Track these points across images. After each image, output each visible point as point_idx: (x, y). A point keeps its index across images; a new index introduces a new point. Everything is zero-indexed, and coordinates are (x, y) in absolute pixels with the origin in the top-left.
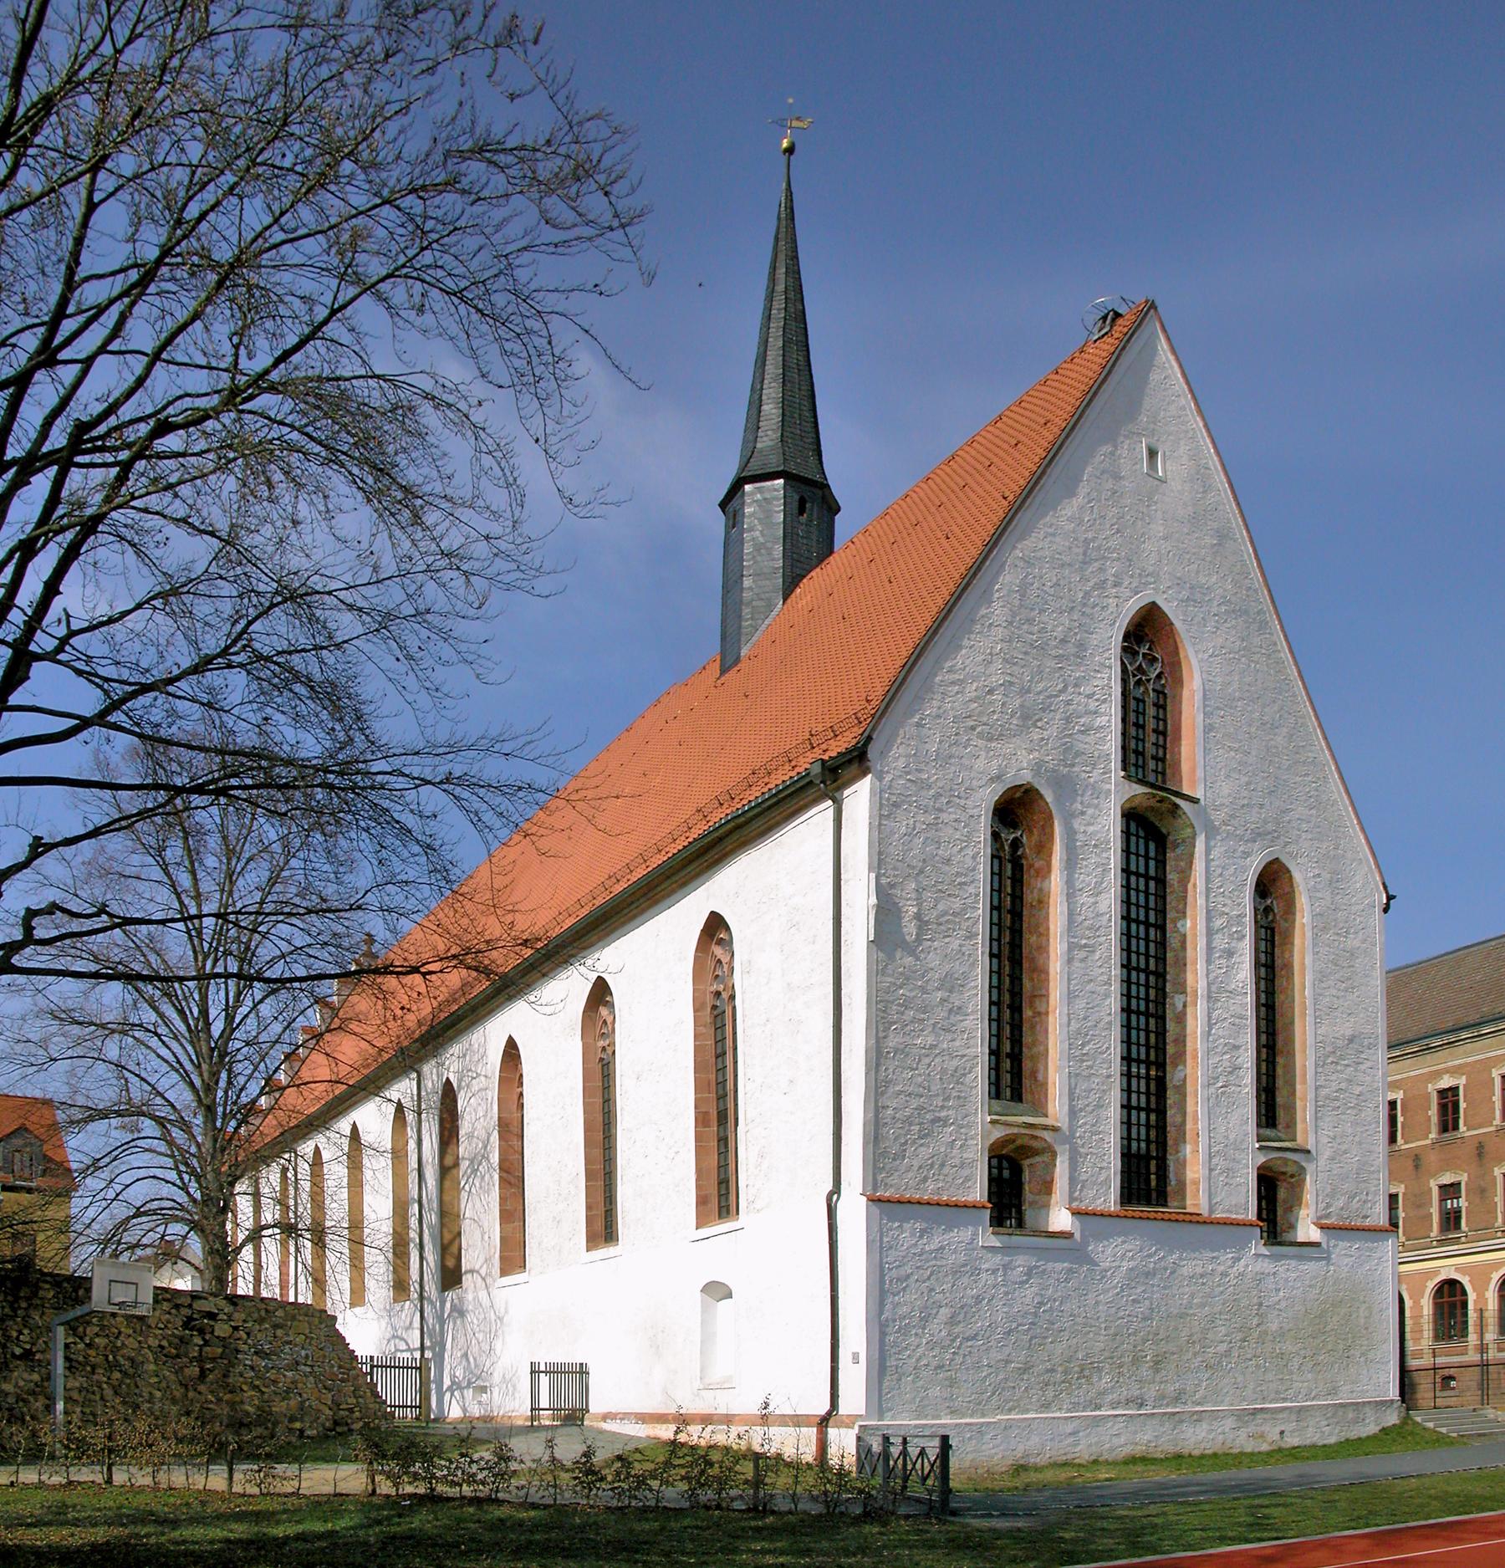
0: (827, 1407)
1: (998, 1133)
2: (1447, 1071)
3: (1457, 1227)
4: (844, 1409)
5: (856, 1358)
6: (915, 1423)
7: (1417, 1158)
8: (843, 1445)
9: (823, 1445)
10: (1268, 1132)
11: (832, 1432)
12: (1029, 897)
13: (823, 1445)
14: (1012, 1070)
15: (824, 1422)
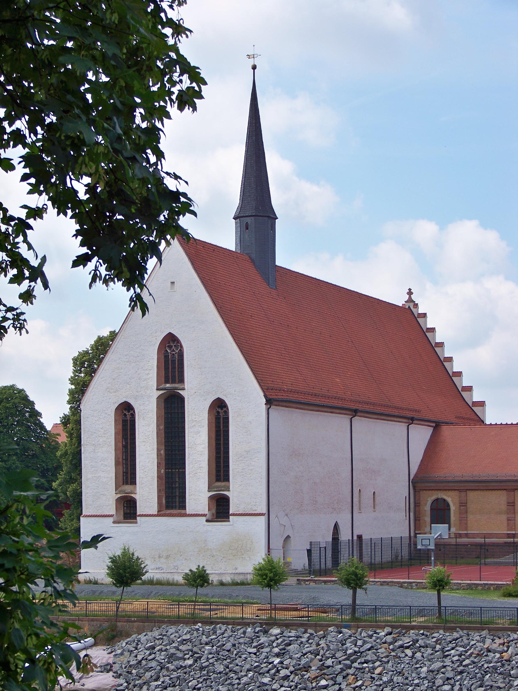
1: (119, 496)
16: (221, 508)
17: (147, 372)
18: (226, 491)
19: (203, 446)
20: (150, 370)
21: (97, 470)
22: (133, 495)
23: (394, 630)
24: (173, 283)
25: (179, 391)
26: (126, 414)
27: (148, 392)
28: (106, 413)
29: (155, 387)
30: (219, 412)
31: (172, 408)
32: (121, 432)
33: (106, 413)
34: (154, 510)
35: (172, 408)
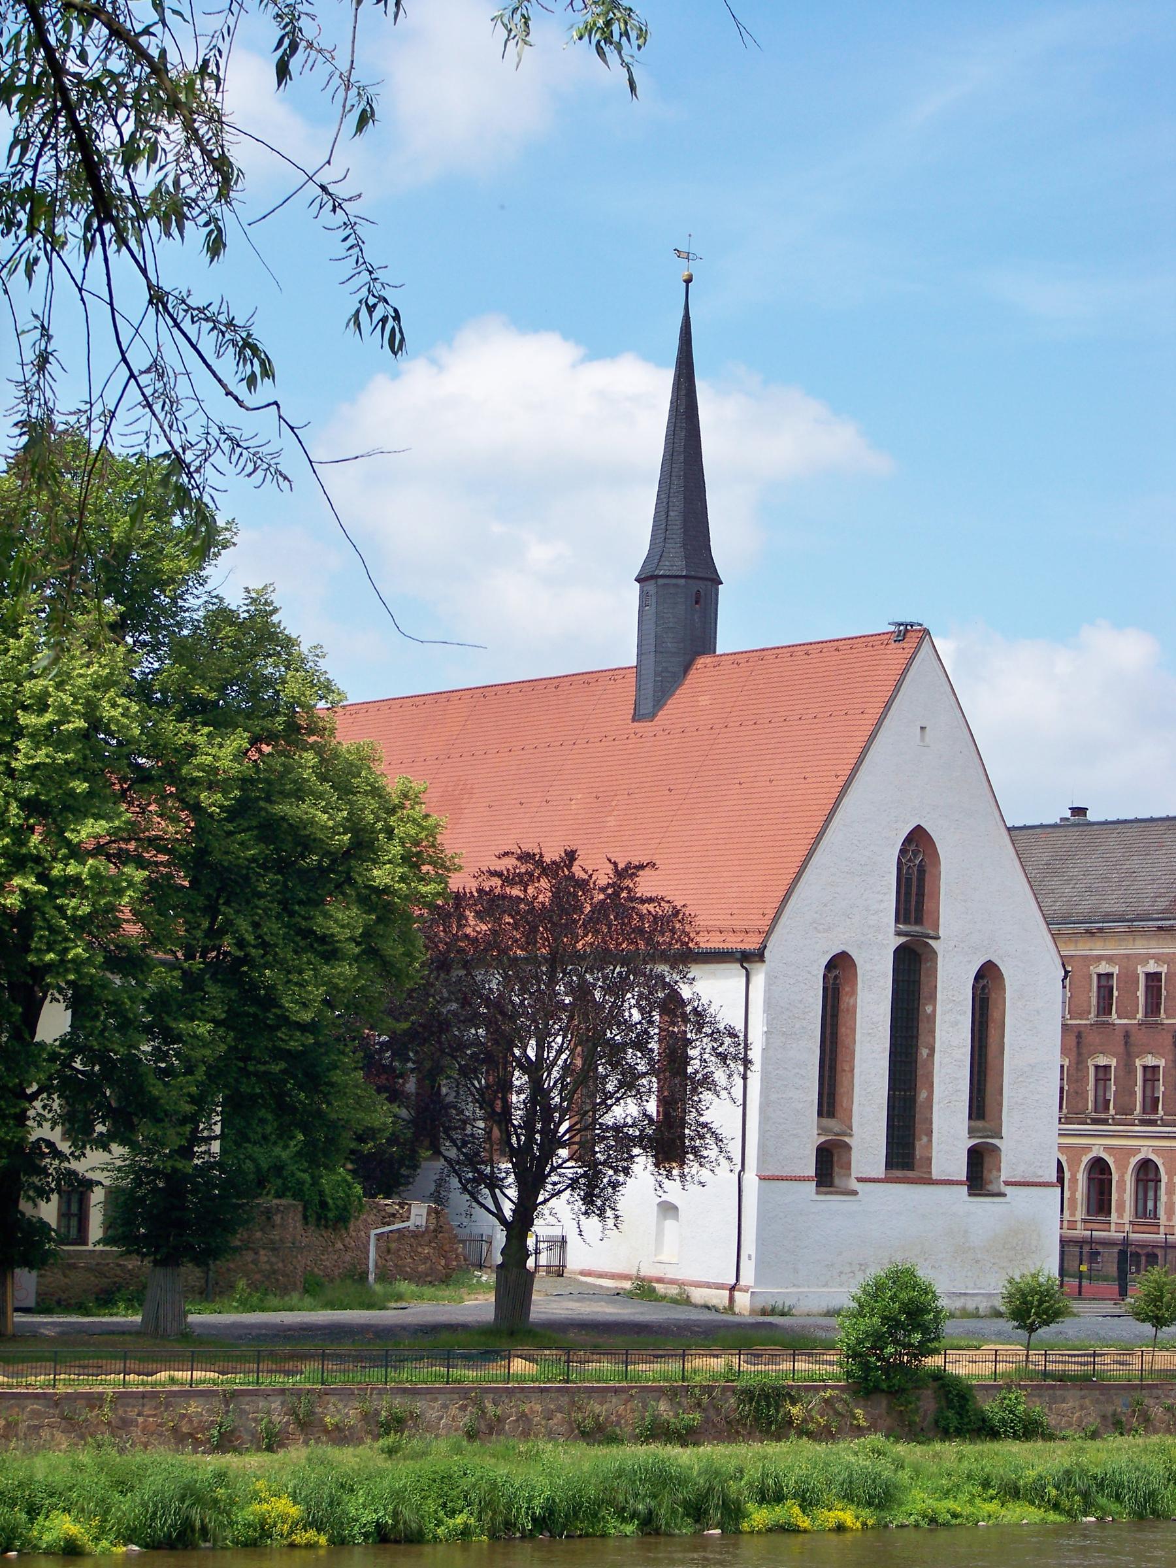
0: (251, 406)
1: (823, 1139)
2: (1153, 956)
3: (1155, 1109)
4: (742, 1283)
5: (750, 1257)
6: (777, 1292)
7: (1127, 1035)
8: (743, 1301)
9: (732, 1299)
10: (979, 1124)
11: (736, 1293)
12: (843, 1006)
13: (732, 1299)
14: (831, 1097)
15: (733, 1289)
16: (980, 1172)
17: (880, 897)
18: (993, 1137)
19: (964, 1050)
20: (885, 894)
21: (786, 1086)
22: (846, 1139)
23: (209, 71)
24: (922, 728)
25: (930, 941)
26: (839, 970)
27: (880, 937)
28: (809, 973)
29: (892, 929)
30: (988, 980)
31: (912, 967)
32: (917, 1133)
33: (809, 973)
34: (880, 1171)
35: (912, 967)
